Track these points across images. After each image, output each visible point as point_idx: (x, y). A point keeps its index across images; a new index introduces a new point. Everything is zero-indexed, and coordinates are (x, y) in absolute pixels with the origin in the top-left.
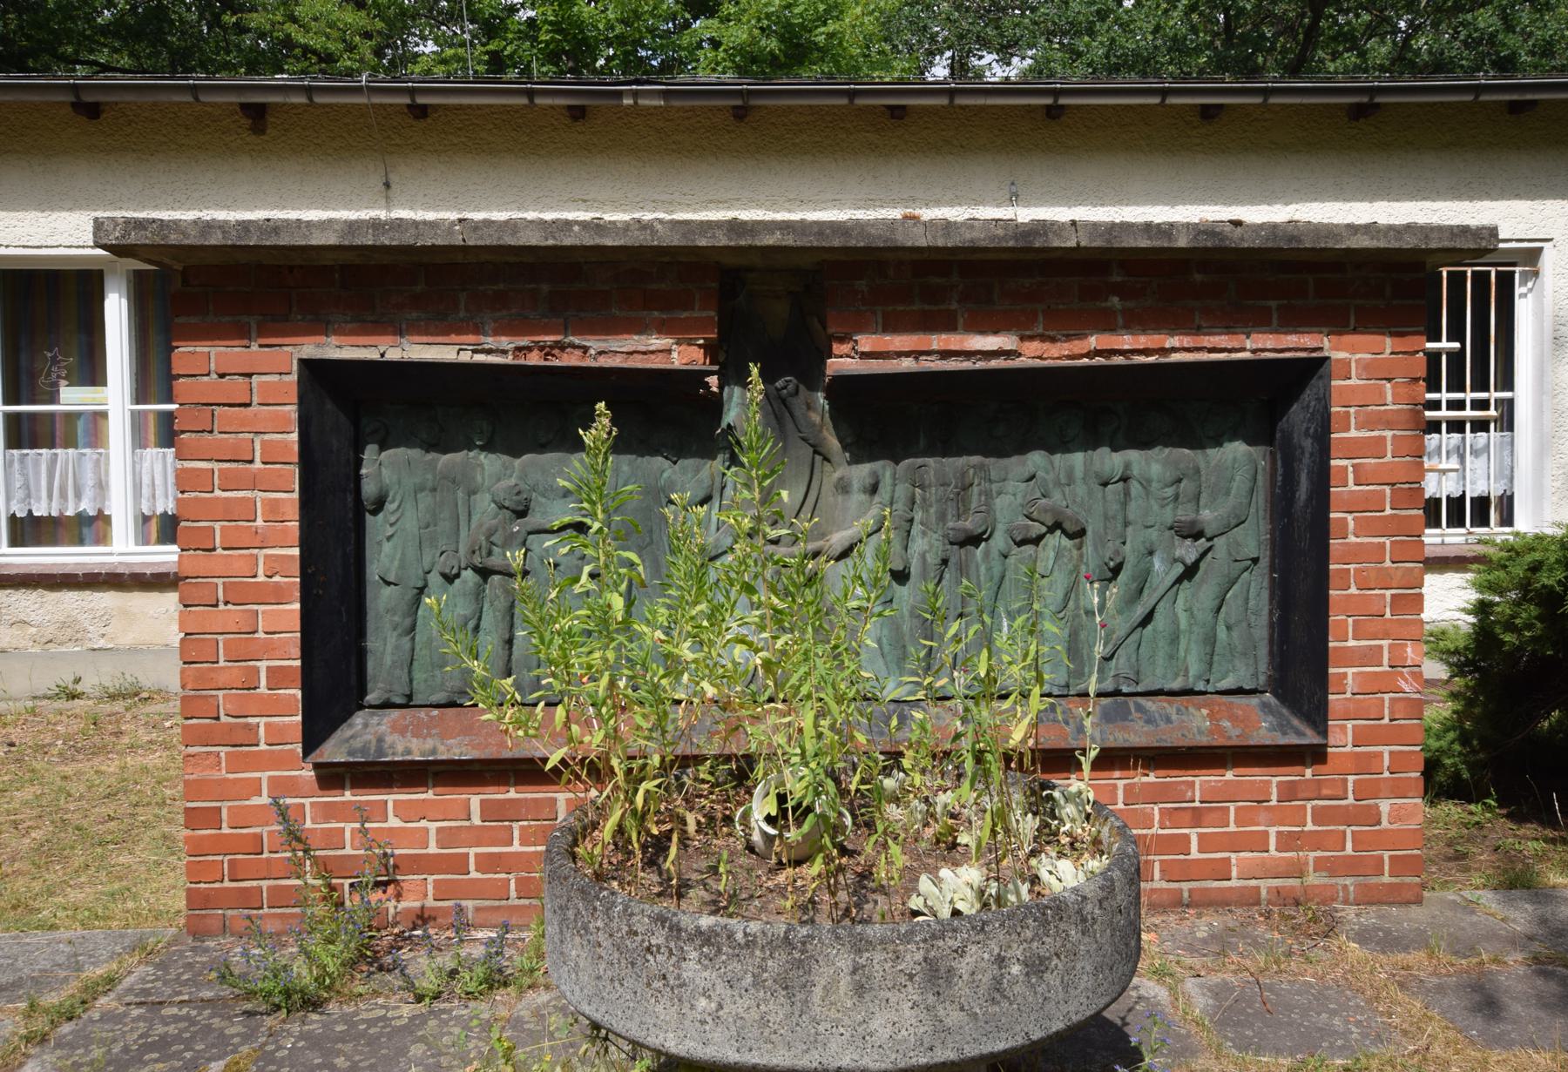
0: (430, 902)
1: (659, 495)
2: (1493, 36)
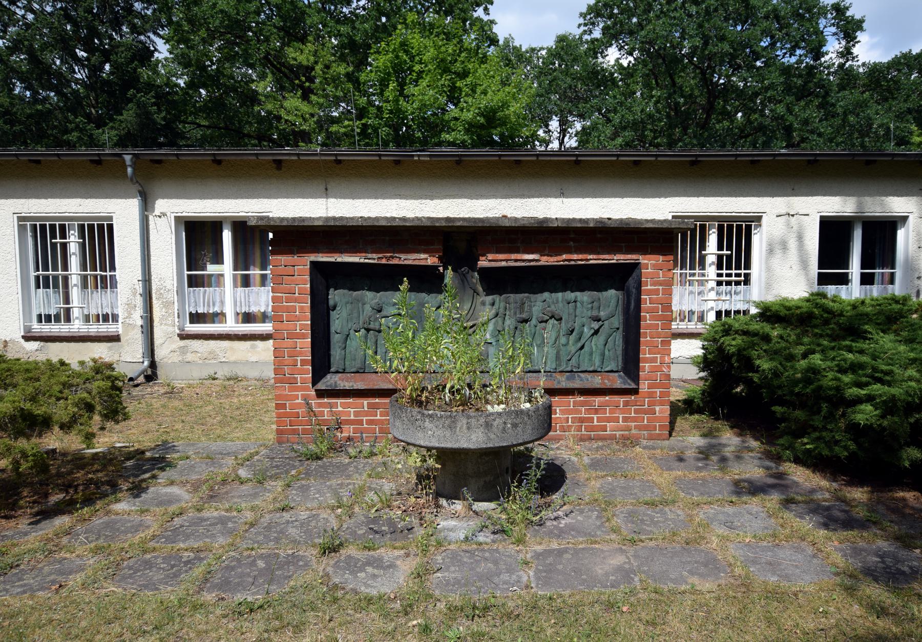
0: (351, 434)
1: (422, 305)
2: (783, 116)
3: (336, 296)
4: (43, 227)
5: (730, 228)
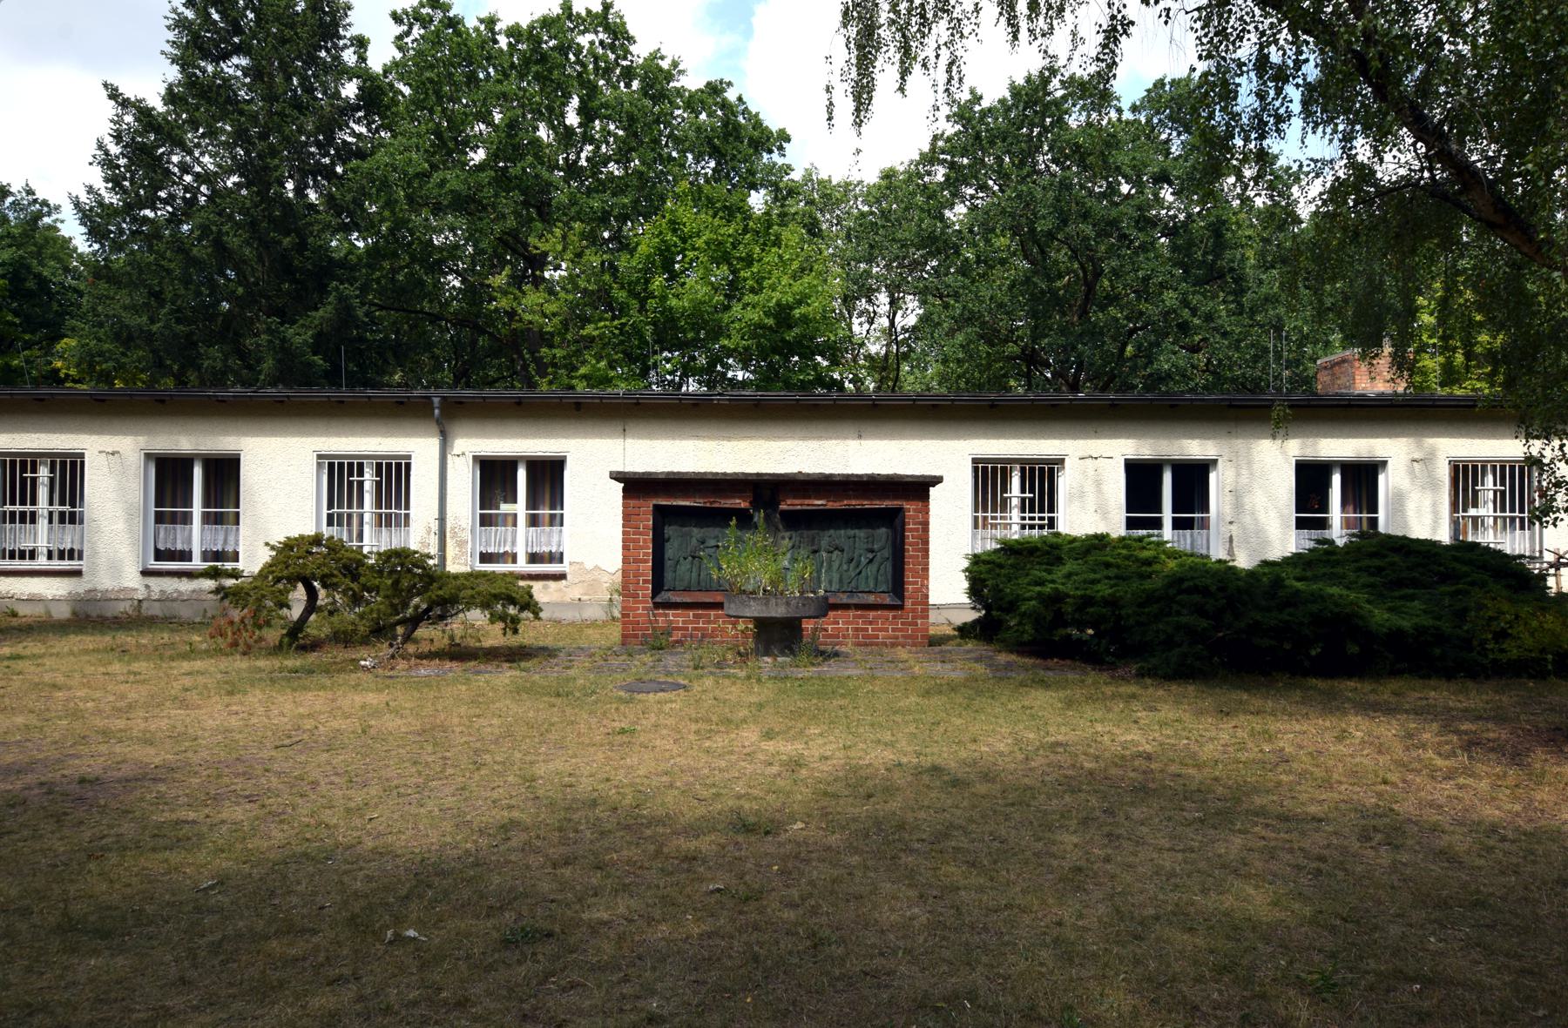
3: (670, 531)
4: (341, 465)
5: (1032, 470)
